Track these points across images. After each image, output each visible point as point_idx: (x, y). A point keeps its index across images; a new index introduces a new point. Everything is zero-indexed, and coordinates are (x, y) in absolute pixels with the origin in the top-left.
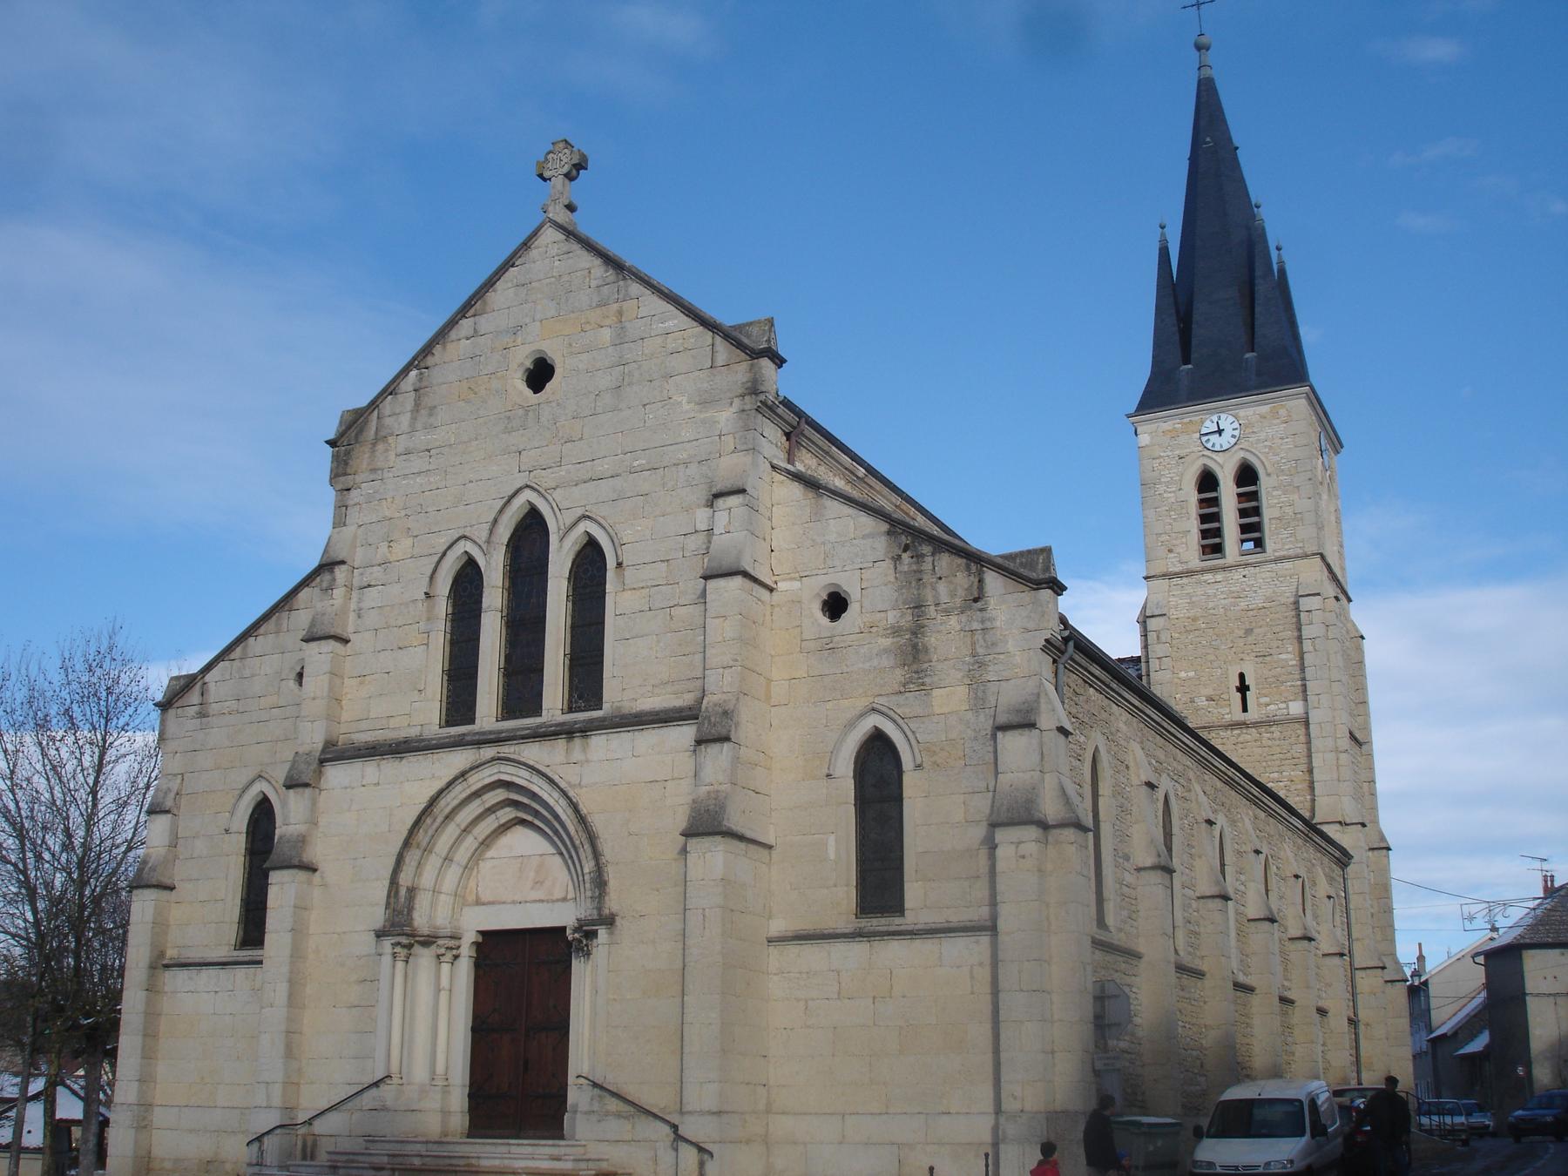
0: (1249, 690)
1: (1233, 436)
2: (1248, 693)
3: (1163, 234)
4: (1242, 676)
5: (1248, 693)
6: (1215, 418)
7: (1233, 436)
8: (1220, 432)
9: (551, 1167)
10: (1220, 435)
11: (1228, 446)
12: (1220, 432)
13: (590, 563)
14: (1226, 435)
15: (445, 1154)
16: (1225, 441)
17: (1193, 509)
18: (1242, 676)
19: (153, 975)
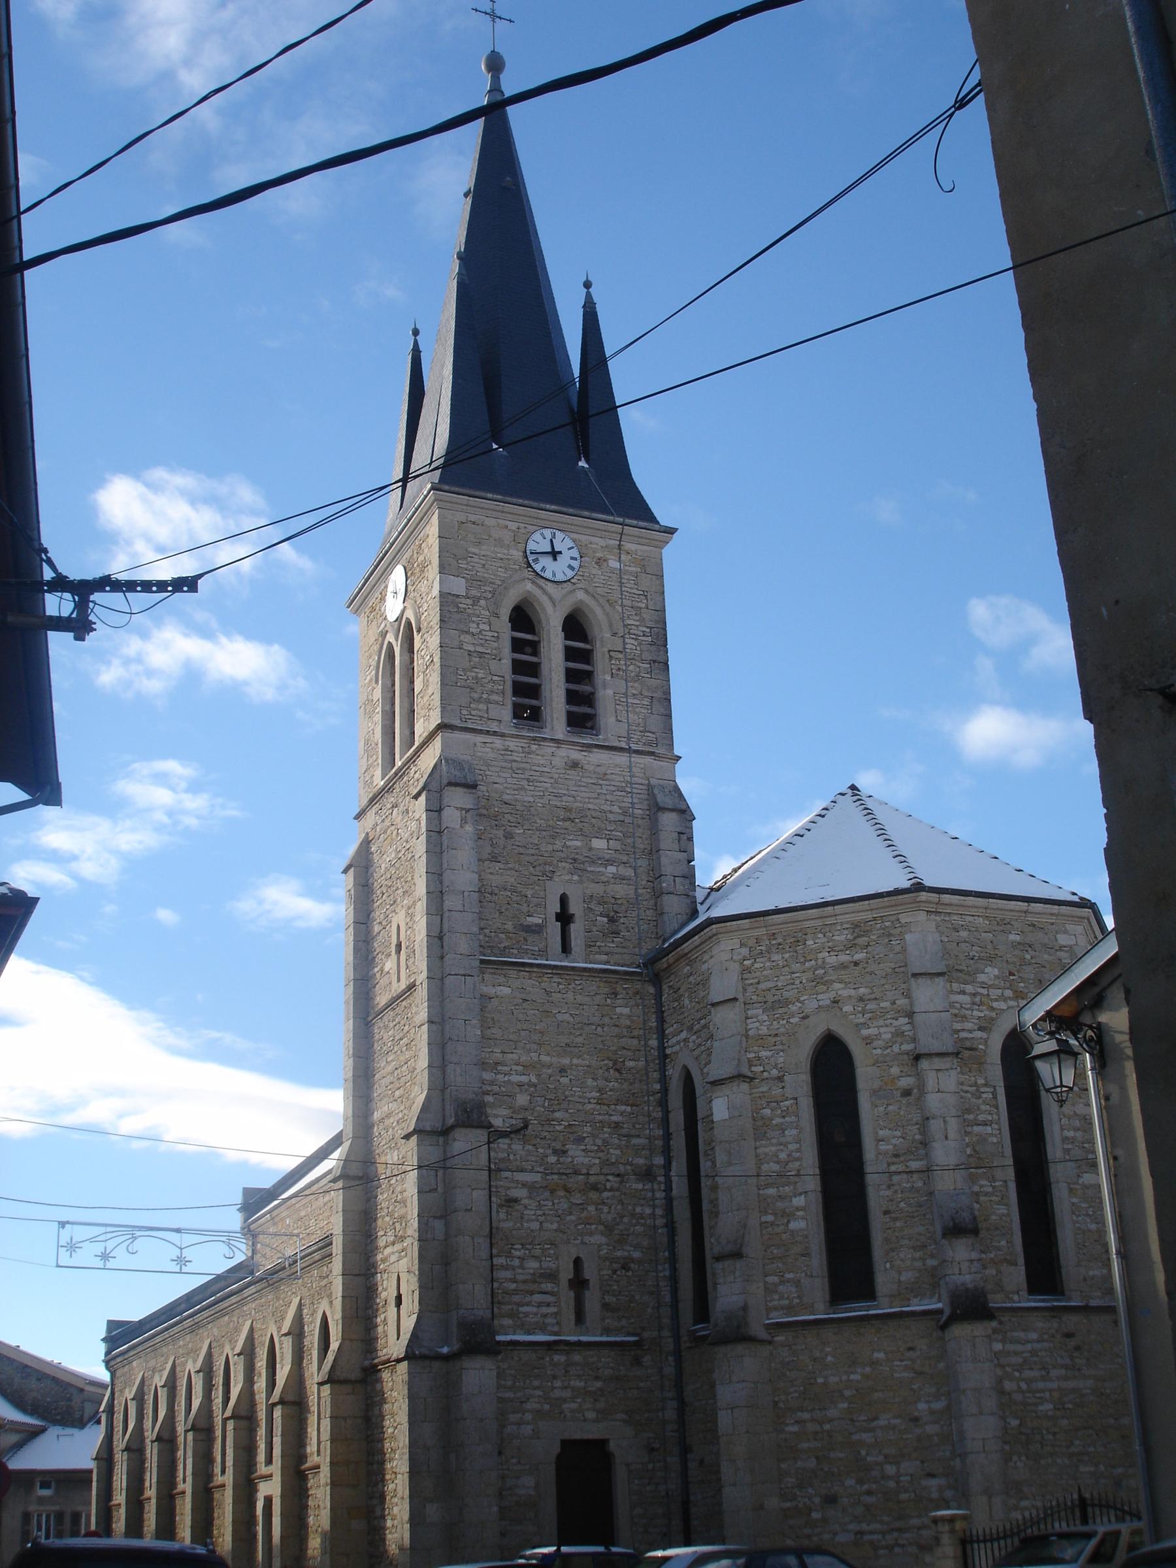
0: (570, 1280)
1: (571, 567)
2: (559, 911)
3: (589, 297)
4: (564, 900)
5: (559, 911)
6: (548, 533)
7: (571, 567)
8: (554, 554)
9: (157, 1545)
10: (555, 559)
11: (563, 578)
12: (554, 554)
13: (575, 626)
14: (564, 560)
15: (307, 1259)
16: (558, 569)
17: (505, 666)
18: (564, 900)
19: (368, 1200)
